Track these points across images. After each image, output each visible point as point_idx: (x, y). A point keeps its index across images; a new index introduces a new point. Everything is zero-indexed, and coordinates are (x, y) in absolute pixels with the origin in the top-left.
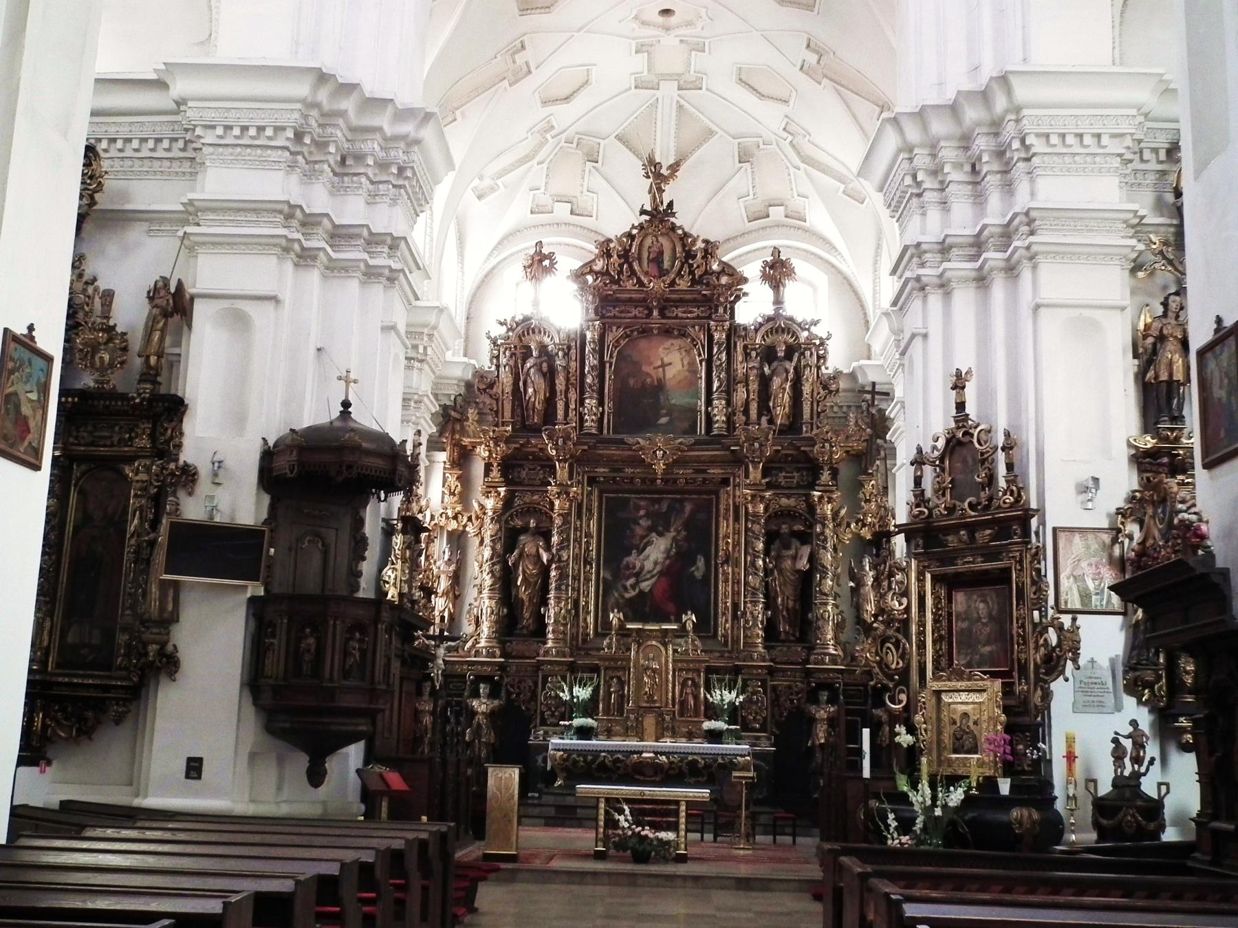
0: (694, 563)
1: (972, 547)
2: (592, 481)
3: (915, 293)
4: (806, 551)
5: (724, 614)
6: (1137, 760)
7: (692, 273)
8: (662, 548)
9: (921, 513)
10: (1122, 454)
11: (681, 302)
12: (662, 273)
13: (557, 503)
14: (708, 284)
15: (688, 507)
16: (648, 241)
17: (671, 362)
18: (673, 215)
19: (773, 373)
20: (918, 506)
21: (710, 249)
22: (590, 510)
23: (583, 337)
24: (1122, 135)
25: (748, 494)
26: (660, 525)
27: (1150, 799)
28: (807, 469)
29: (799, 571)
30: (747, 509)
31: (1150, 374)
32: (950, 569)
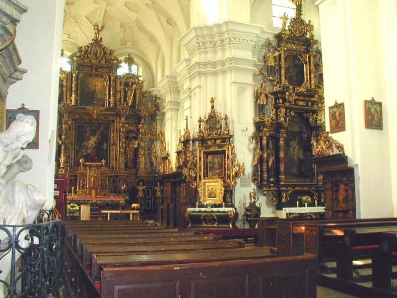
0: (103, 145)
1: (215, 144)
2: (74, 119)
3: (198, 76)
4: (137, 142)
5: (112, 160)
6: (255, 198)
7: (106, 59)
8: (94, 140)
9: (201, 135)
10: (252, 122)
11: (102, 67)
12: (97, 58)
13: (64, 126)
14: (110, 63)
15: (102, 128)
16: (93, 48)
17: (98, 84)
18: (102, 41)
19: (128, 90)
20: (200, 133)
21: (111, 52)
22: (73, 128)
23: (72, 76)
24: (252, 41)
25: (120, 125)
26: (93, 133)
27: (258, 207)
28: (137, 118)
29: (135, 148)
30: (120, 130)
31: (258, 102)
32: (208, 150)
